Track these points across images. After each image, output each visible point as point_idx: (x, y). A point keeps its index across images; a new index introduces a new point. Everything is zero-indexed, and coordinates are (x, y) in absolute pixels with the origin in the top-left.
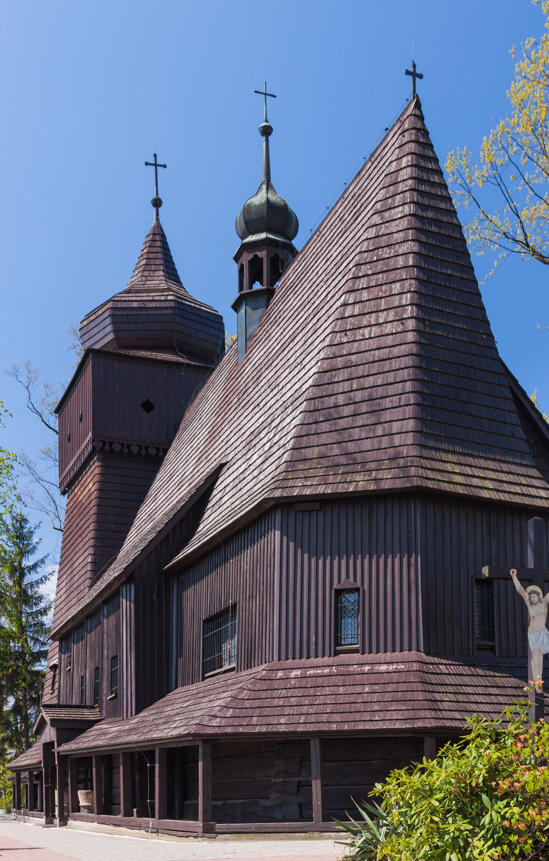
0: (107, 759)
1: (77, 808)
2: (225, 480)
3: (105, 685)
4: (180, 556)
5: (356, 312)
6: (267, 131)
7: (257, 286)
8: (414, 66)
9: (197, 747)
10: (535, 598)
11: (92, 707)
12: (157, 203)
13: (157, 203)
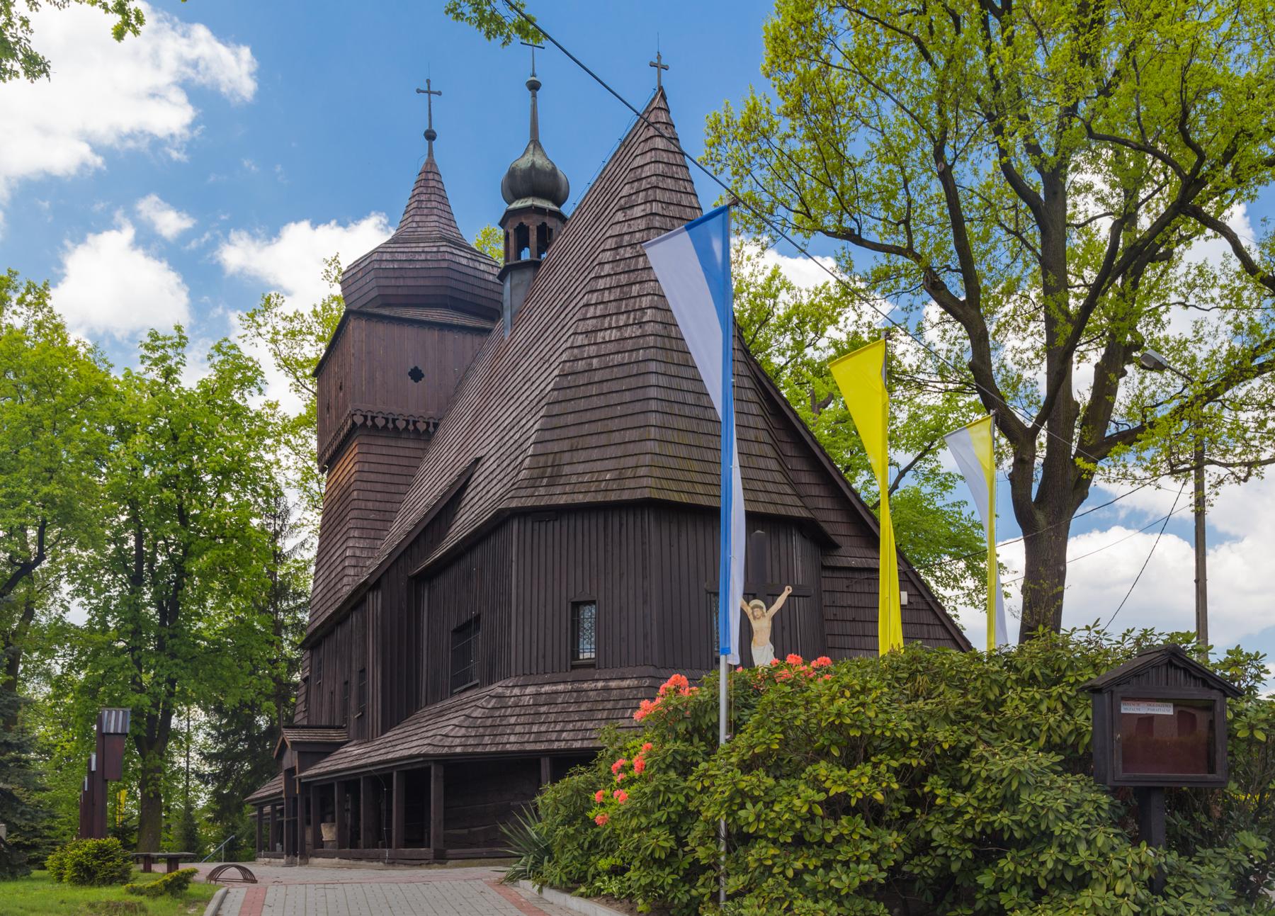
0: (350, 782)
1: (319, 842)
2: (479, 477)
3: (353, 703)
4: (430, 560)
5: (598, 313)
6: (534, 86)
7: (526, 255)
8: (659, 57)
9: (430, 768)
10: (758, 612)
11: (340, 727)
12: (430, 136)
13: (430, 136)
